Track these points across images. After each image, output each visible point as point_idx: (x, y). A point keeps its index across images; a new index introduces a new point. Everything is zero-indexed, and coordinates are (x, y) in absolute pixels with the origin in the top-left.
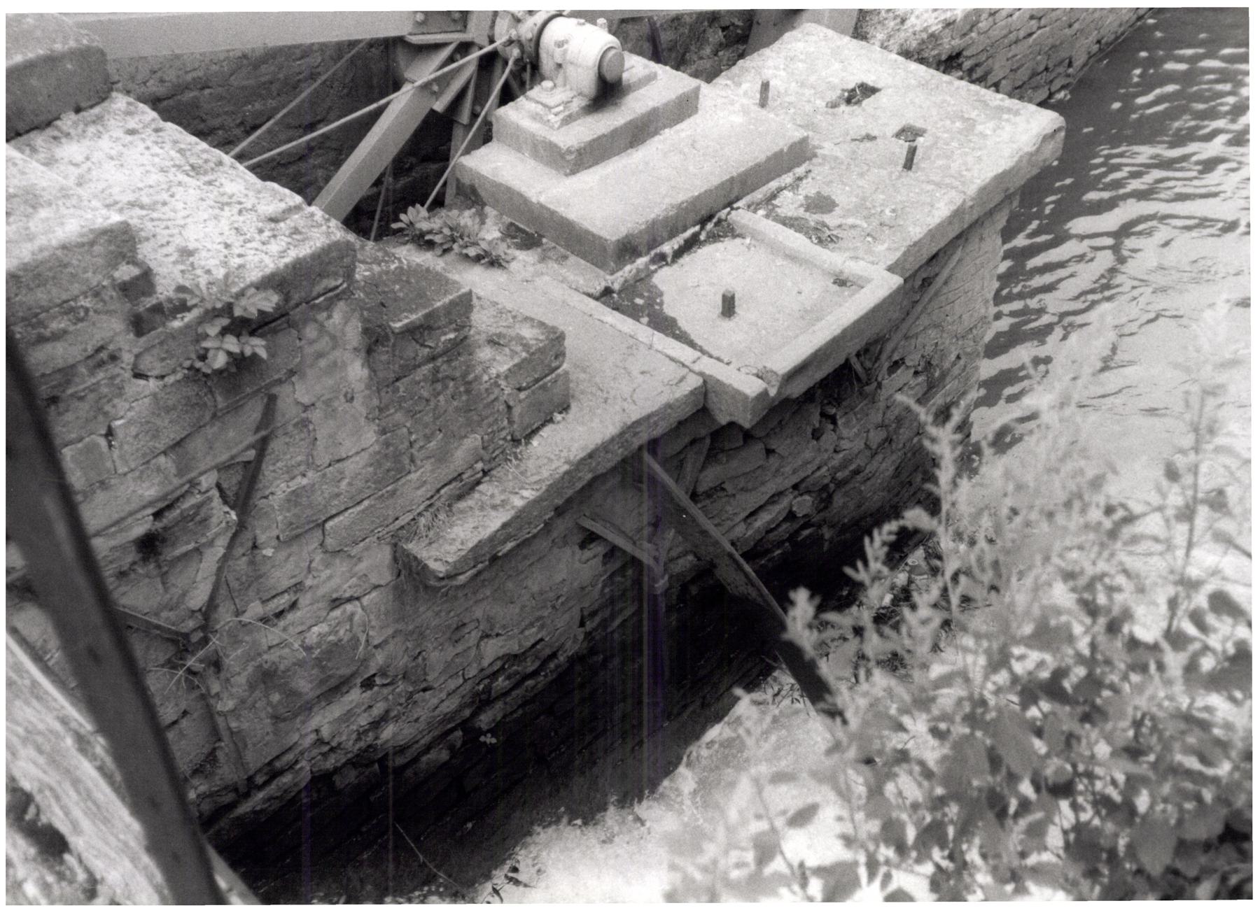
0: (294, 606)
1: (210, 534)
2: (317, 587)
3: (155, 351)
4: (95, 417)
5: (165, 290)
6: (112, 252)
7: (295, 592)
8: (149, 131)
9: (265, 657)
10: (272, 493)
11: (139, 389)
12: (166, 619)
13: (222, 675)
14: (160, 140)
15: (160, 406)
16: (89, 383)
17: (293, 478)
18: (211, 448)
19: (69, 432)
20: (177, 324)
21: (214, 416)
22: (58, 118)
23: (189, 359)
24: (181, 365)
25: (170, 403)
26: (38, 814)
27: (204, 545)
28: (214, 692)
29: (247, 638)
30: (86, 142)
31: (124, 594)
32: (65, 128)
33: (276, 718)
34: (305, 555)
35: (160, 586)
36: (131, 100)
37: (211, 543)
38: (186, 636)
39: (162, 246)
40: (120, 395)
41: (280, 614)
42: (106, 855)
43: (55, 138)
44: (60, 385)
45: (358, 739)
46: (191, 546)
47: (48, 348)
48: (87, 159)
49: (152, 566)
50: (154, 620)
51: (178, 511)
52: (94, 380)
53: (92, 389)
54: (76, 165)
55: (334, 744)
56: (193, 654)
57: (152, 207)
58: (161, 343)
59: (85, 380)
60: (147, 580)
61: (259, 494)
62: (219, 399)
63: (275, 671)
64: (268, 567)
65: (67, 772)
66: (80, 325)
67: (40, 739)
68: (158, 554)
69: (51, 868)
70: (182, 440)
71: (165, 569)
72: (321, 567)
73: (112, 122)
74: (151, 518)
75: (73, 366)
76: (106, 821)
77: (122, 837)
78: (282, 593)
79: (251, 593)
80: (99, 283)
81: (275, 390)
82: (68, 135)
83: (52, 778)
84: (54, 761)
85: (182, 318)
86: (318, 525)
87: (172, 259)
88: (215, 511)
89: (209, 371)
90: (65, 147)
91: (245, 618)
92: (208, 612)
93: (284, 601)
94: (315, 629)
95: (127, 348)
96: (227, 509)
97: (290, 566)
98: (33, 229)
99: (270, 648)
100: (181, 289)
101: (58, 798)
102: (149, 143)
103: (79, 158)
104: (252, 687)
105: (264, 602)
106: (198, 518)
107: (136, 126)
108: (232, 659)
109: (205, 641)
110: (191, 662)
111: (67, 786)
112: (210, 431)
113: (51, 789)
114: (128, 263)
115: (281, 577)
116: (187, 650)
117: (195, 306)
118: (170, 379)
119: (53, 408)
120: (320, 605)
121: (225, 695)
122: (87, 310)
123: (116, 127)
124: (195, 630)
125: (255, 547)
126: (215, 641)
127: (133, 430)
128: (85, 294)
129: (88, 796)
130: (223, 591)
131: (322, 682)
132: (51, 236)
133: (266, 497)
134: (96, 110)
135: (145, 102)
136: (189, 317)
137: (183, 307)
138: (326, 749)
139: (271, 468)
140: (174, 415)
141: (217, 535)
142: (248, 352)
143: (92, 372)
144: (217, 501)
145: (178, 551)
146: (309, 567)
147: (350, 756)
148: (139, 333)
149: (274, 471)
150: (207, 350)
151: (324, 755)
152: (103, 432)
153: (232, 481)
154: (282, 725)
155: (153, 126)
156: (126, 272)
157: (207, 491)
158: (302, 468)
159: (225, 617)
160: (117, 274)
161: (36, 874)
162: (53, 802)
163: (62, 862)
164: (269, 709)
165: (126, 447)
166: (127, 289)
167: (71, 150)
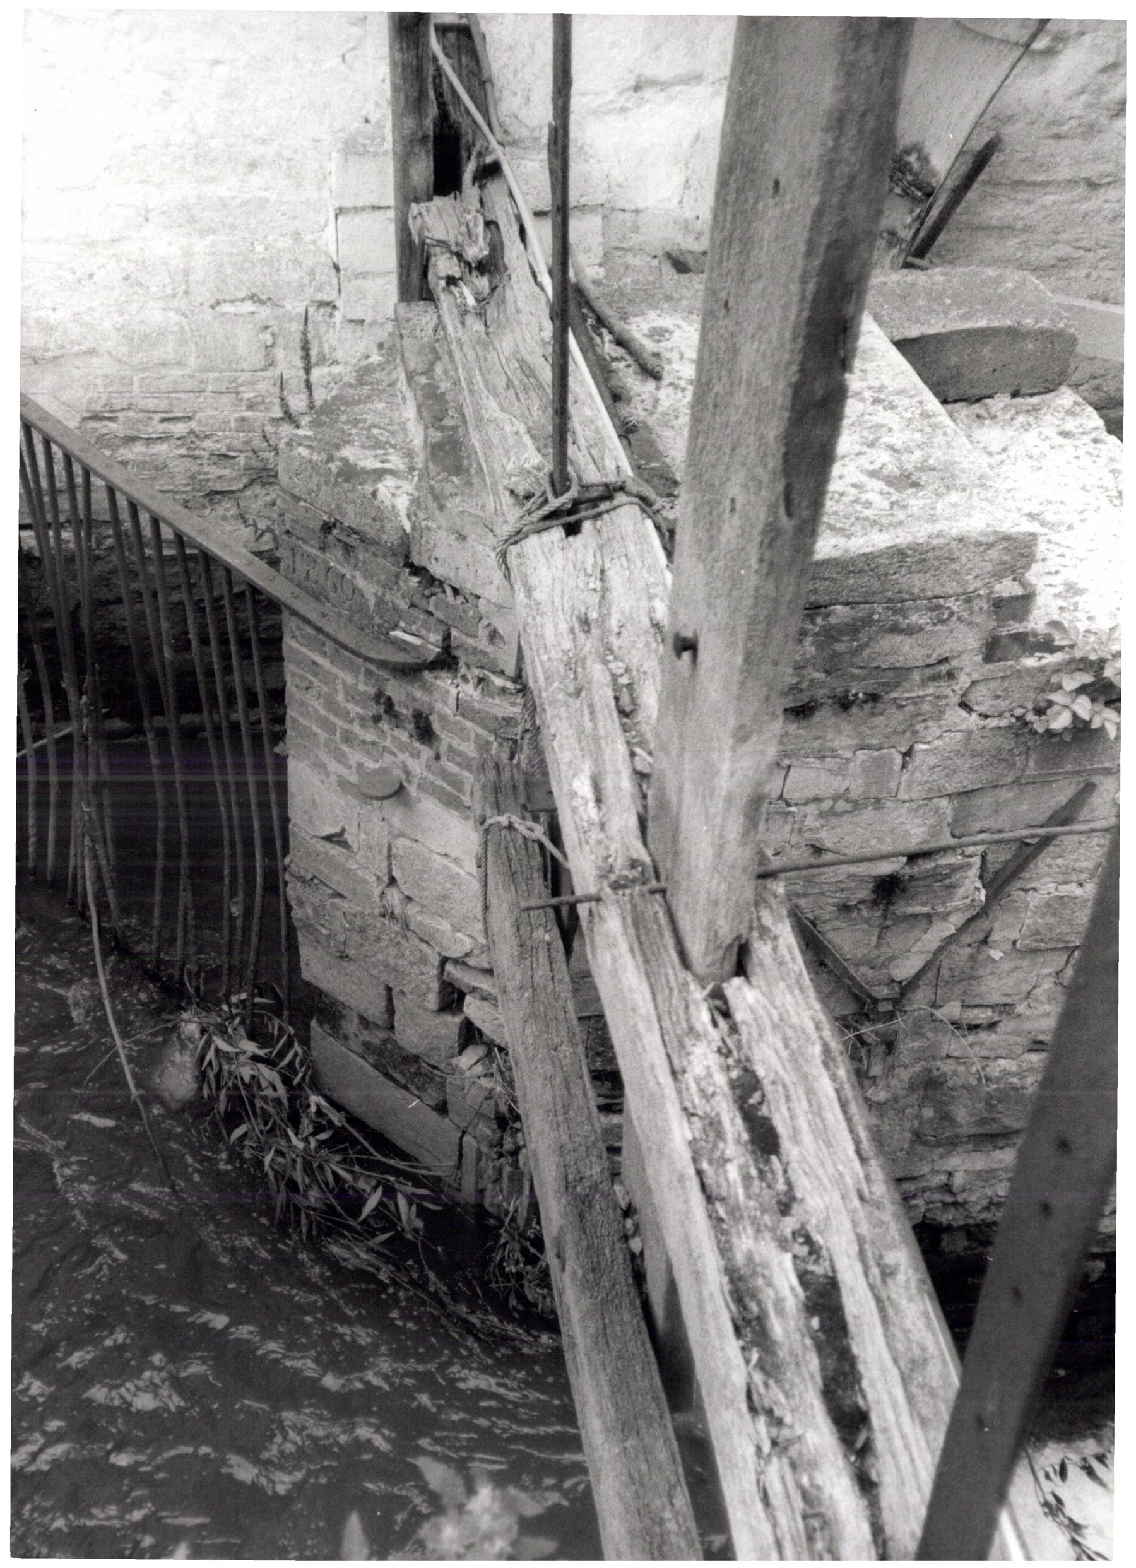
0: (992, 1026)
1: (950, 905)
2: (1028, 1018)
3: (993, 685)
4: (904, 732)
5: (1037, 622)
6: (1004, 563)
7: (1001, 1013)
8: (1087, 439)
9: (939, 1063)
10: (1034, 889)
11: (957, 720)
12: (863, 974)
13: (890, 1059)
14: (1095, 453)
15: (968, 748)
16: (913, 694)
17: (1066, 883)
18: (996, 812)
19: (872, 736)
20: (1030, 662)
21: (1016, 781)
22: (990, 397)
23: (1022, 707)
24: (1011, 710)
25: (979, 748)
26: (761, 1103)
27: (938, 914)
28: (872, 1073)
29: (929, 1035)
30: (1010, 432)
31: (836, 929)
32: (993, 410)
33: (918, 1136)
34: (1032, 979)
35: (874, 939)
36: (1080, 400)
37: (945, 916)
38: (875, 1001)
39: (1050, 573)
40: (939, 719)
41: (973, 1028)
42: (818, 1178)
43: (978, 416)
44: (887, 684)
45: (987, 1209)
46: (925, 910)
47: (898, 638)
48: (1004, 450)
49: (879, 913)
50: (852, 971)
51: (933, 864)
52: (921, 693)
53: (916, 701)
54: (990, 454)
55: (960, 1199)
56: (873, 1022)
57: (1052, 527)
58: (1003, 678)
59: (914, 689)
60: (865, 926)
61: (1018, 884)
62: (1032, 764)
63: (942, 1084)
64: (988, 970)
65: (805, 1077)
66: (939, 627)
67: (790, 1033)
68: (890, 903)
69: (756, 1161)
70: (972, 791)
71: (889, 923)
72: (1043, 998)
73: (1049, 417)
74: (905, 859)
75: (910, 669)
76: (829, 1145)
77: (840, 1168)
78: (991, 1006)
79: (958, 990)
80: (976, 590)
81: (1096, 779)
82: (994, 417)
83: (789, 1078)
84: (796, 1061)
85: (1040, 658)
86: (1066, 948)
87: (1056, 591)
88: (967, 882)
89: (1041, 730)
90: (985, 429)
91: (939, 1014)
92: (907, 987)
93: (983, 1016)
94: (1002, 1062)
95: (967, 670)
96: (979, 884)
97: (1011, 981)
98: (939, 511)
99: (948, 1057)
100: (1055, 624)
101: (788, 1098)
102: (1081, 452)
103: (995, 447)
104: (912, 1087)
105: (965, 1006)
106: (947, 882)
107: (1075, 430)
108: (907, 1047)
109: (891, 1016)
110: (866, 1030)
111: (801, 1091)
112: (1006, 794)
113: (785, 1087)
114: (1014, 579)
115: (993, 988)
116: (867, 1016)
117: (1061, 649)
118: (992, 723)
119: (870, 705)
120: (1019, 1040)
121: (881, 1083)
122: (952, 614)
123: (1049, 423)
124: (886, 1000)
125: (985, 941)
126: (900, 1022)
127: (932, 760)
128: (957, 596)
129: (817, 1111)
130: (930, 975)
131: (983, 1122)
132: (955, 524)
133: (1026, 891)
134: (1035, 400)
135: (1091, 404)
136: (1050, 659)
137: (1048, 646)
138: (948, 1199)
139: (1049, 861)
140: (977, 762)
141: (957, 909)
142: (1095, 724)
143: (924, 683)
144: (974, 872)
145: (910, 910)
146: (1029, 993)
147: (971, 1221)
148: (988, 658)
149: (1050, 866)
150: (1050, 704)
151: (945, 1204)
152: (904, 750)
153: (1000, 857)
154: (919, 1148)
155: (1093, 435)
156: (1007, 588)
157: (970, 856)
158: (1084, 876)
159: (919, 1000)
160: (998, 587)
161: (742, 1160)
162: (783, 1101)
163: (767, 1162)
164: (916, 1123)
165: (917, 775)
166: (998, 604)
167: (991, 435)
